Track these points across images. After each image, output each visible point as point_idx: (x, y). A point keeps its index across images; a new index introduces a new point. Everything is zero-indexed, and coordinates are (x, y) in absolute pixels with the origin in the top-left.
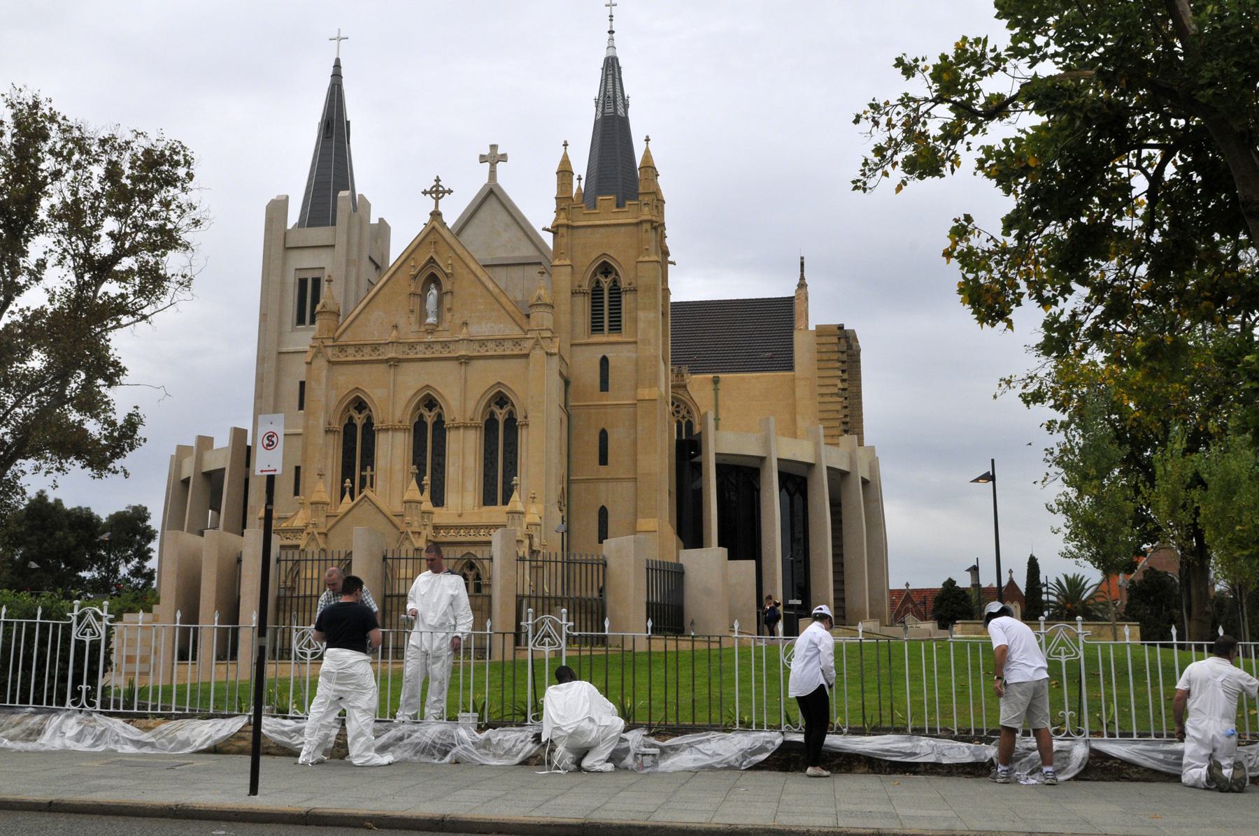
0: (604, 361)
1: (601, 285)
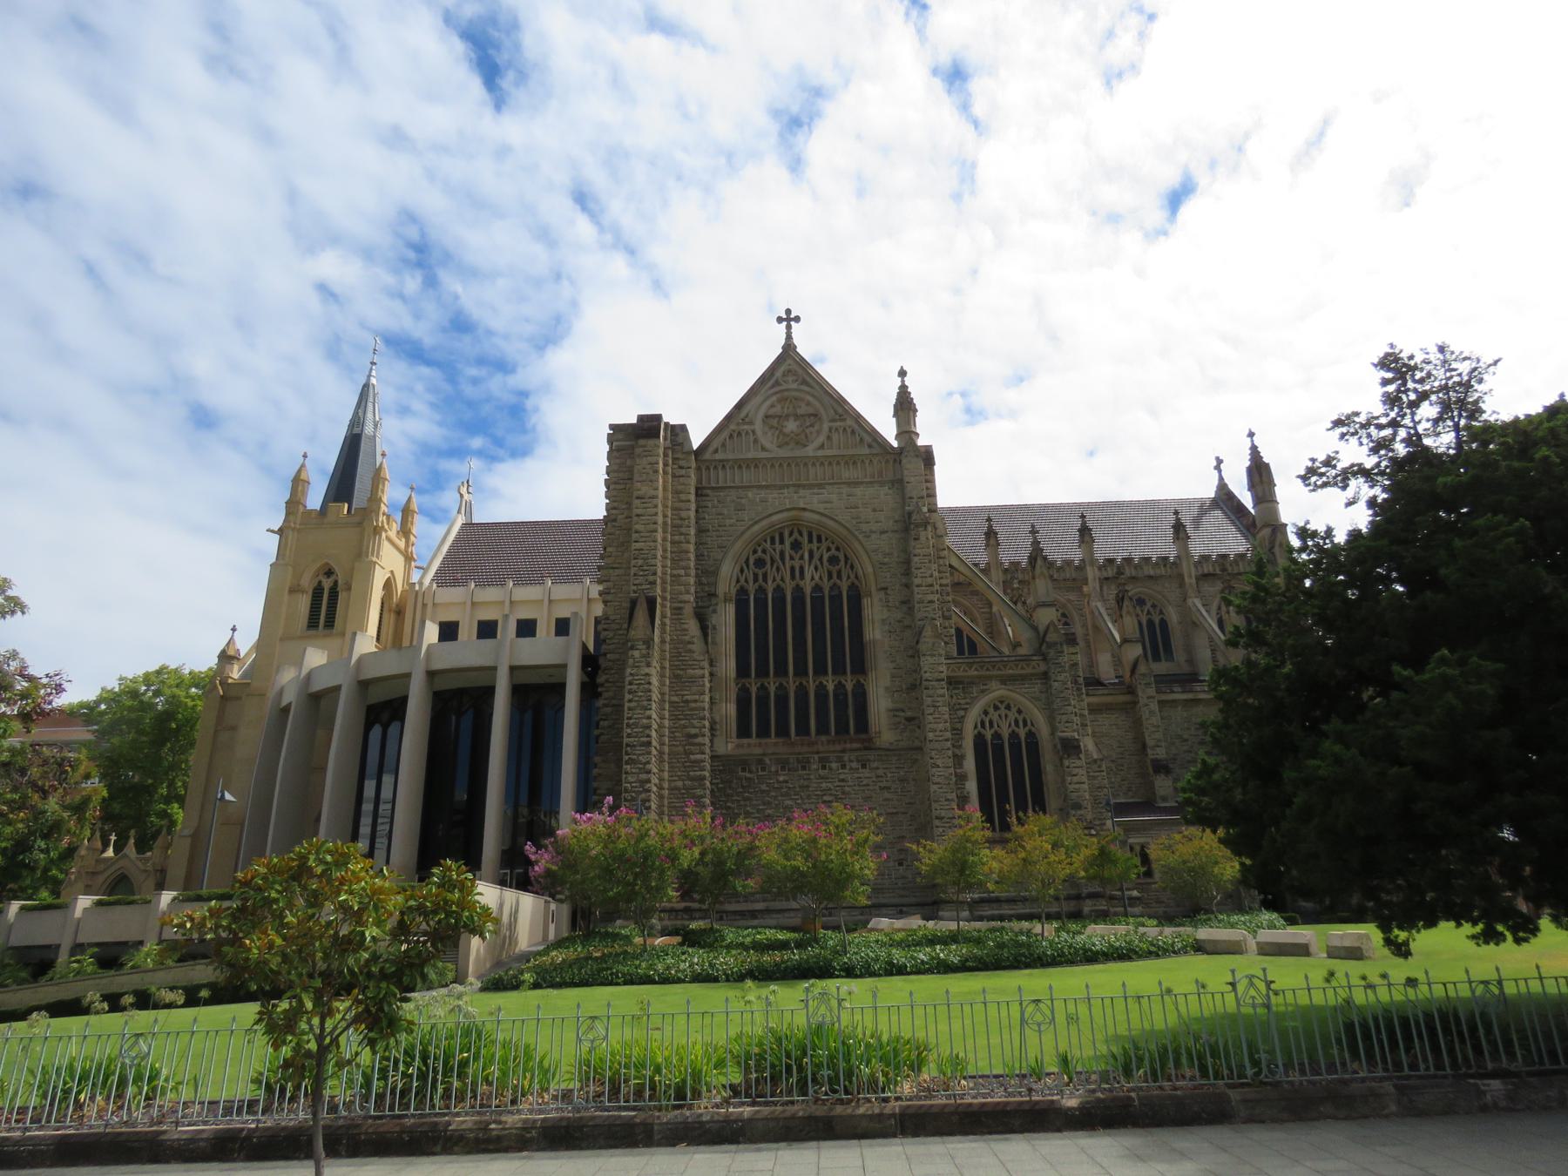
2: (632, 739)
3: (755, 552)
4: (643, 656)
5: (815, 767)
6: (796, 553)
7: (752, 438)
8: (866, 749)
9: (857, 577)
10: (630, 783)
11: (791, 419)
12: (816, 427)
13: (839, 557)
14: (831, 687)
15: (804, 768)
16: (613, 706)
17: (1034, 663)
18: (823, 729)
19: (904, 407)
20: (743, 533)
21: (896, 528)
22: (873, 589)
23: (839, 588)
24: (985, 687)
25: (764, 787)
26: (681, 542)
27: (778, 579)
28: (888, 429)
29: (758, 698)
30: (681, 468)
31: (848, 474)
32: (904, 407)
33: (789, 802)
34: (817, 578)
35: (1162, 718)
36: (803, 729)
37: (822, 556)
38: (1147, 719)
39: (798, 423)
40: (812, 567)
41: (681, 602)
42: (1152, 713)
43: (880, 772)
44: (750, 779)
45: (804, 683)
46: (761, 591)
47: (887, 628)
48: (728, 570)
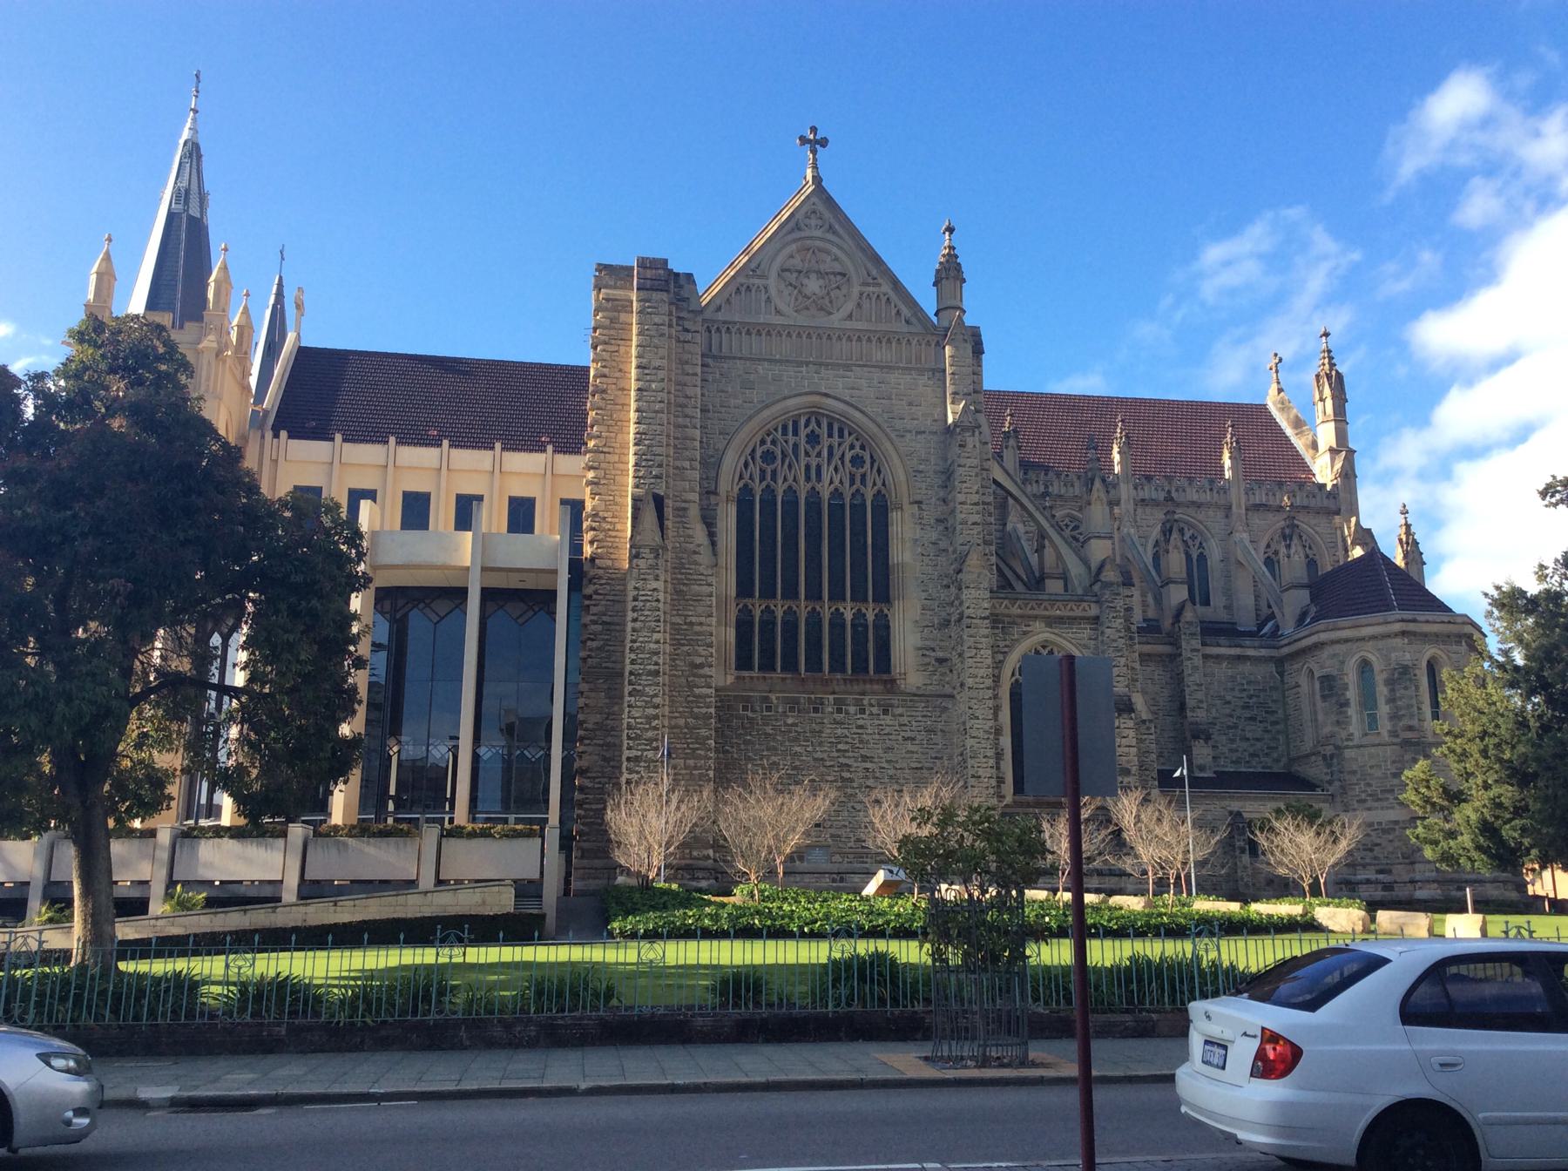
2: (637, 667)
3: (763, 442)
4: (651, 567)
5: (830, 709)
6: (813, 448)
7: (764, 297)
8: (889, 692)
9: (884, 484)
10: (635, 718)
11: (813, 276)
12: (844, 291)
13: (864, 458)
14: (848, 616)
15: (816, 710)
16: (604, 623)
17: (1085, 604)
18: (837, 664)
19: (950, 273)
20: (750, 418)
21: (934, 429)
22: (905, 501)
23: (863, 495)
24: (1028, 629)
25: (769, 730)
26: (686, 427)
27: (790, 479)
28: (928, 301)
29: (784, 623)
30: (687, 331)
31: (880, 354)
32: (950, 273)
33: (798, 749)
34: (837, 482)
35: (1205, 675)
36: (814, 664)
37: (843, 455)
38: (1189, 675)
39: (821, 282)
40: (832, 468)
41: (685, 501)
42: (1195, 668)
43: (905, 720)
44: (752, 719)
45: (818, 608)
46: (769, 491)
48: (731, 462)
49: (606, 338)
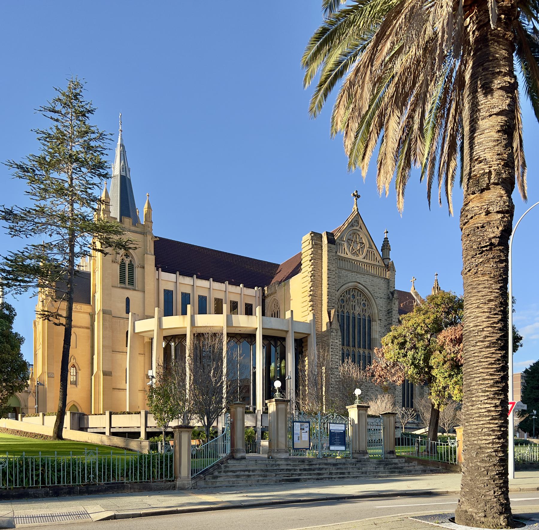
0: (128, 300)
1: (124, 261)
3: (341, 296)
21: (384, 297)
45: (354, 350)
46: (343, 312)
47: (380, 334)
49: (315, 258)
